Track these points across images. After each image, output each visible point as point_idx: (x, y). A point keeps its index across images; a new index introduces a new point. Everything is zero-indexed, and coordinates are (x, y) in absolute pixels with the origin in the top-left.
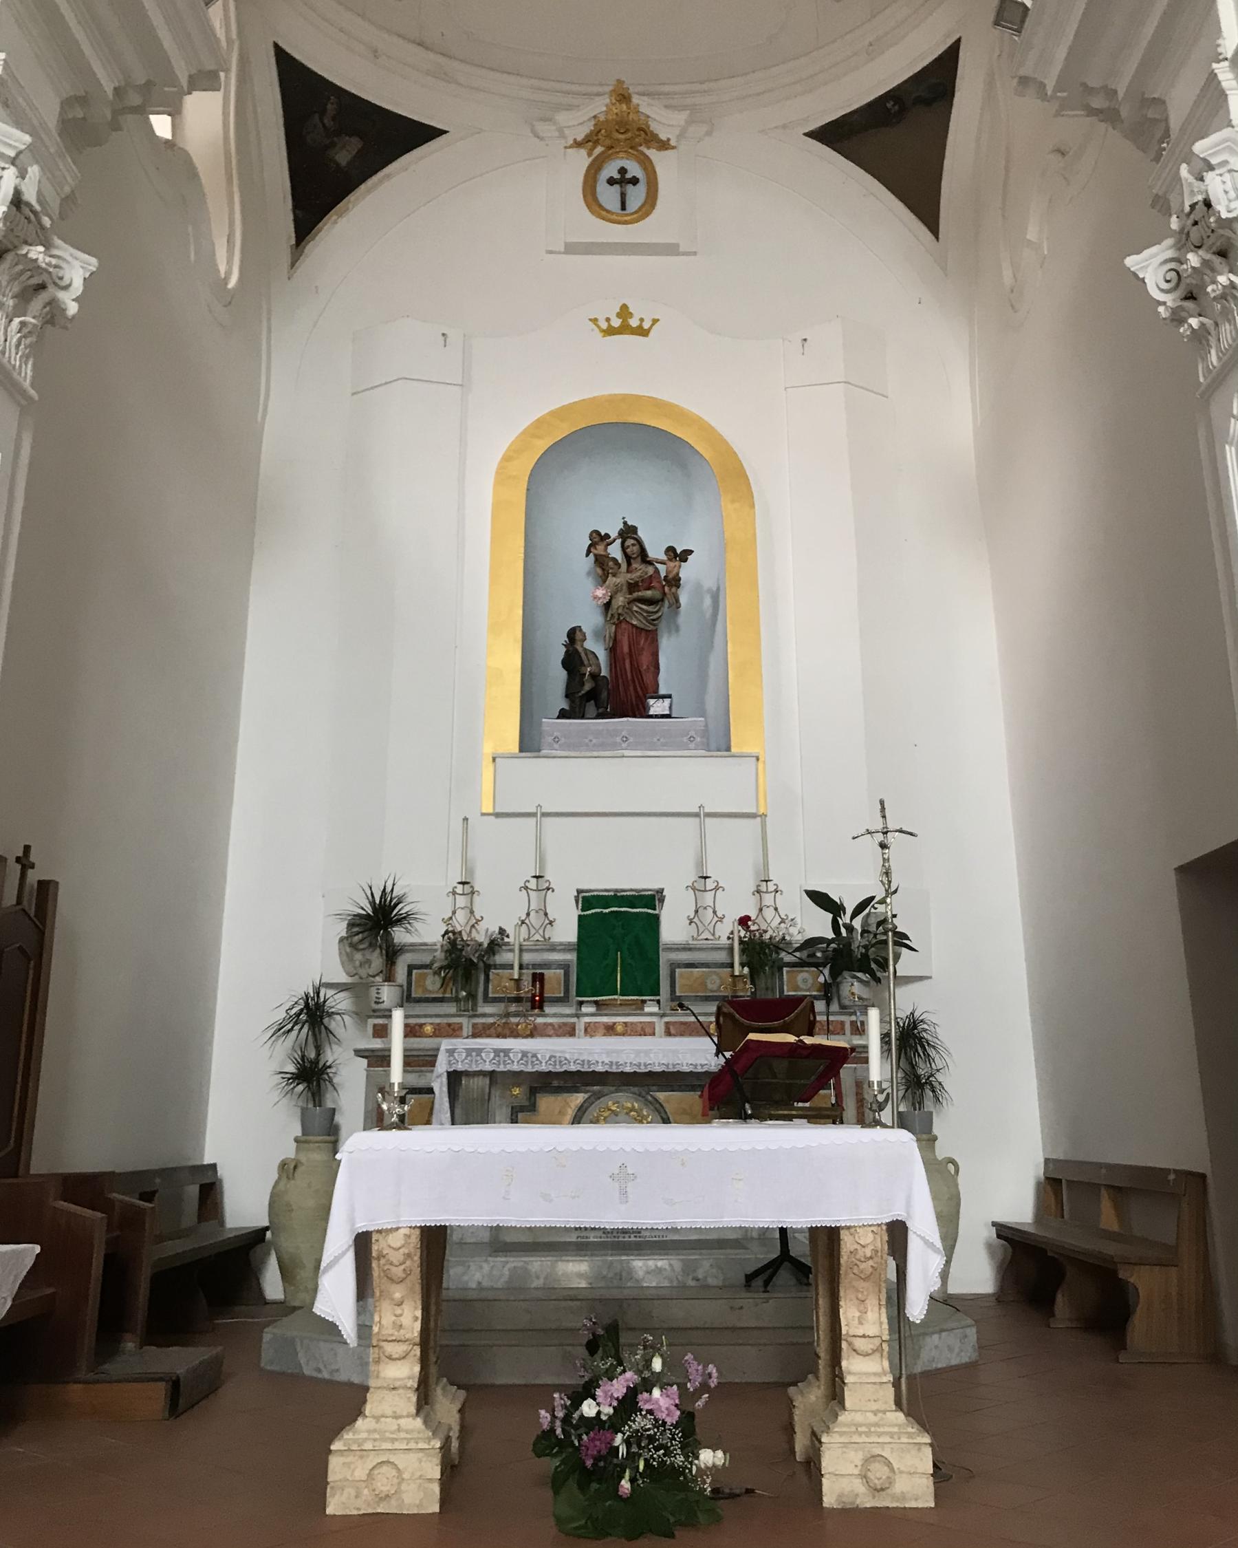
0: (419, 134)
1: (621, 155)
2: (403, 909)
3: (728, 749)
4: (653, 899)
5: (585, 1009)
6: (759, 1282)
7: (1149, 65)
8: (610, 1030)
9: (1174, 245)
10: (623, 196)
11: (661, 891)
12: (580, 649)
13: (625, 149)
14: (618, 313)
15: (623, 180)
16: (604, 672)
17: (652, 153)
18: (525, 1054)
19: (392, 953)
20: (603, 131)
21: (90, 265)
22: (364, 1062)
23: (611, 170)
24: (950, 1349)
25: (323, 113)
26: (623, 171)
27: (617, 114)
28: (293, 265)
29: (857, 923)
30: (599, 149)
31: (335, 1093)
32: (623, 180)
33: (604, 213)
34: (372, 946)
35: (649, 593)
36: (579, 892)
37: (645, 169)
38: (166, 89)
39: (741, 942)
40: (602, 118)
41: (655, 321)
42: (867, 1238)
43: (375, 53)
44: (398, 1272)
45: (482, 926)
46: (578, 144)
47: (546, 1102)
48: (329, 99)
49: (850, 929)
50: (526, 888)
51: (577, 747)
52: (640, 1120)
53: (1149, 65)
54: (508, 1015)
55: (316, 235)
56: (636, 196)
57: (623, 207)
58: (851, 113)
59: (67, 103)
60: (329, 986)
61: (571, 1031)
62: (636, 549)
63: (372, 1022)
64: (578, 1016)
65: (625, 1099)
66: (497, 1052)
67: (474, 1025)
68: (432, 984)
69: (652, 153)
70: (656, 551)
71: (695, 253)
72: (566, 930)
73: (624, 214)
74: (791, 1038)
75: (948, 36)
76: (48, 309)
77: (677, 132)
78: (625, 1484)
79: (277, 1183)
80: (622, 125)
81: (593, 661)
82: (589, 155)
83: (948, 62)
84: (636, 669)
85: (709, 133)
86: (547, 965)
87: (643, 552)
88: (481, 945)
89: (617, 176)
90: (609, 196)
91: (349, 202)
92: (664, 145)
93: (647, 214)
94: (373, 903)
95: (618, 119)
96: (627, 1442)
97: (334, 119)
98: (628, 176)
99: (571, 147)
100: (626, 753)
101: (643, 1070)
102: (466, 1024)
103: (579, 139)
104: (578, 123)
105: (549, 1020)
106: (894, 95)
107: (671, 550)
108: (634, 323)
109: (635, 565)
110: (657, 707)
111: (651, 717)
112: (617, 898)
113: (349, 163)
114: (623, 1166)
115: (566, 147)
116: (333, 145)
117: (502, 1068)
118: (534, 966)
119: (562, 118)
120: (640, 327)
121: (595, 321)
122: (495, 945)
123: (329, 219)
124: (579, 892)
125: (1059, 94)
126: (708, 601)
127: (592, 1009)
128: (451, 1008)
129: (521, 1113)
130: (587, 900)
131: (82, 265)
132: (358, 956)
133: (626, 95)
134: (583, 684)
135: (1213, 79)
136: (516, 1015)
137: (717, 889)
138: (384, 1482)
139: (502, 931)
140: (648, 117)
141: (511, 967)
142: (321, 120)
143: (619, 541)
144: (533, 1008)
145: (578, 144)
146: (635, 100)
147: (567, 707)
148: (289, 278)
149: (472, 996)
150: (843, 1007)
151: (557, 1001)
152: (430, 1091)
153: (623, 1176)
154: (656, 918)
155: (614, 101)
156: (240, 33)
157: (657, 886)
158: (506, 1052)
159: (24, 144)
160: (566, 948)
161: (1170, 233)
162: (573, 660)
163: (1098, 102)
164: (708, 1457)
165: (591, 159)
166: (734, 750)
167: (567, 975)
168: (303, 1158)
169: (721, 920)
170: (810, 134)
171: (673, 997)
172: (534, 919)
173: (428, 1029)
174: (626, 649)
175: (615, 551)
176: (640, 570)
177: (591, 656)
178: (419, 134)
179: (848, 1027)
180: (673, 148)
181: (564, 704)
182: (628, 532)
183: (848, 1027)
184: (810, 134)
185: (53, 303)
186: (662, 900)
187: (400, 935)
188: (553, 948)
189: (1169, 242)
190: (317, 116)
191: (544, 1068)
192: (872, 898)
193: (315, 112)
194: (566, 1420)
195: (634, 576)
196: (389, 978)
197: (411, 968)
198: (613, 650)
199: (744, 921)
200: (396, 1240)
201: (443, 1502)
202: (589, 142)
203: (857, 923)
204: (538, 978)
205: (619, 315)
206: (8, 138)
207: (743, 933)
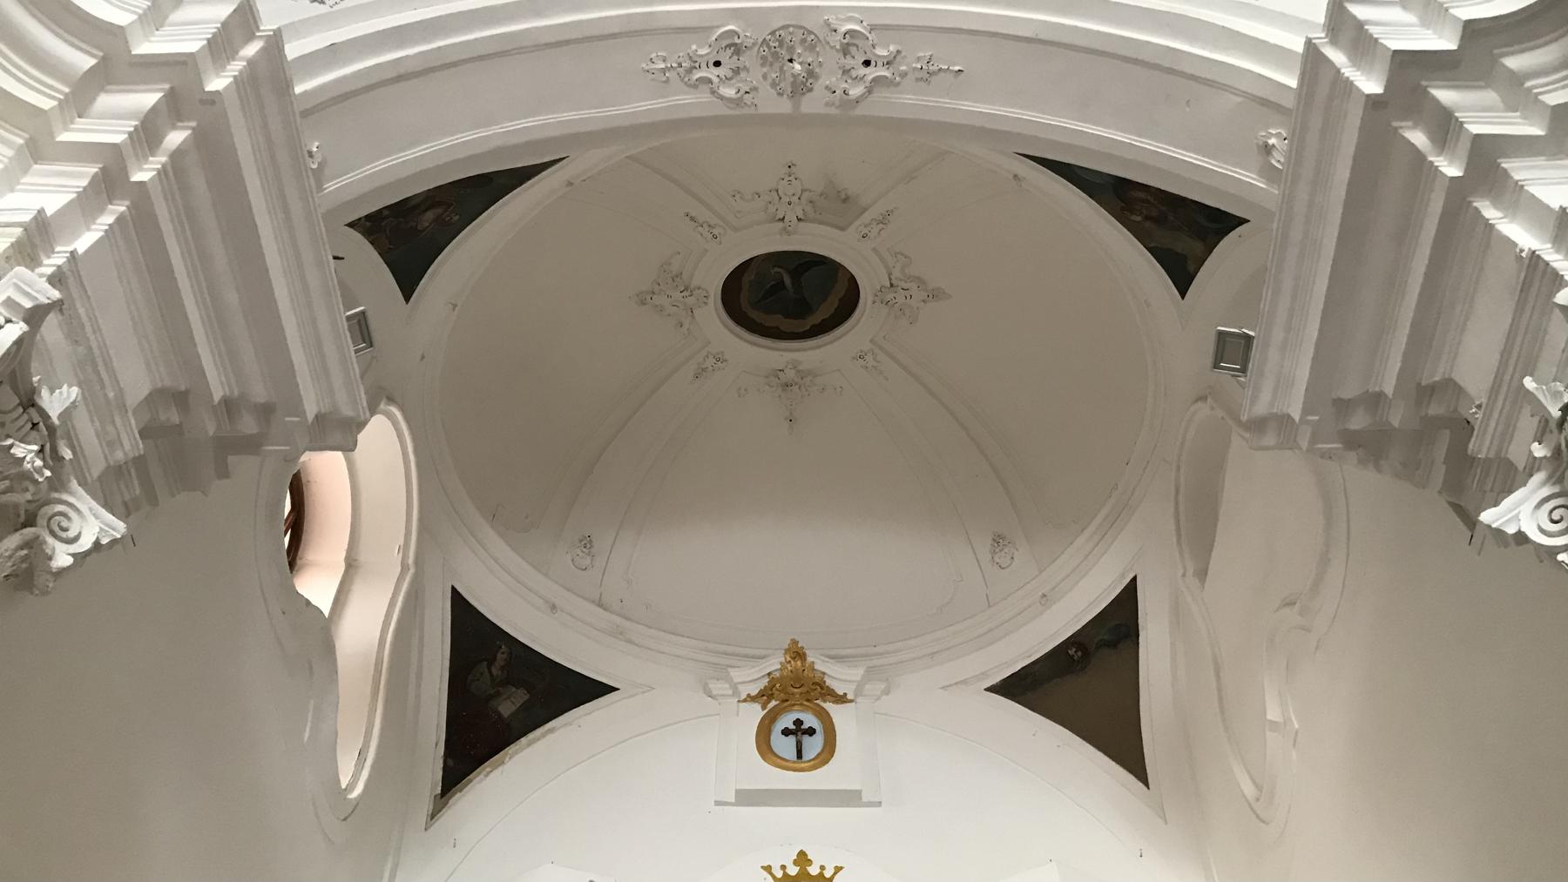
0: (589, 690)
1: (796, 707)
7: (1423, 340)
9: (1549, 478)
13: (801, 701)
14: (795, 860)
15: (799, 731)
20: (778, 686)
21: (114, 529)
23: (787, 721)
25: (491, 663)
26: (798, 722)
27: (791, 671)
28: (433, 816)
30: (773, 703)
32: (799, 731)
33: (779, 760)
38: (287, 419)
40: (778, 674)
41: (838, 869)
43: (554, 607)
46: (751, 699)
48: (500, 647)
53: (1423, 340)
55: (466, 785)
56: (813, 746)
57: (799, 755)
58: (1033, 663)
59: (158, 396)
71: (879, 804)
75: (1123, 576)
76: (25, 552)
77: (853, 687)
82: (764, 708)
83: (1128, 598)
85: (887, 692)
89: (792, 727)
90: (785, 746)
91: (506, 755)
92: (841, 699)
93: (825, 762)
95: (792, 676)
97: (502, 668)
98: (806, 726)
99: (745, 701)
103: (754, 693)
104: (752, 678)
106: (1075, 641)
113: (512, 715)
115: (739, 701)
116: (498, 694)
119: (737, 675)
120: (821, 875)
121: (768, 869)
123: (484, 770)
125: (1310, 418)
131: (103, 526)
133: (801, 652)
135: (1537, 264)
140: (824, 673)
145: (751, 699)
148: (426, 829)
155: (789, 659)
156: (416, 562)
159: (48, 298)
161: (1533, 466)
163: (1358, 421)
165: (765, 711)
170: (991, 689)
178: (589, 690)
180: (851, 701)
184: (991, 689)
185: (33, 545)
189: (1538, 477)
193: (483, 660)
202: (764, 696)
205: (795, 863)
206: (30, 286)
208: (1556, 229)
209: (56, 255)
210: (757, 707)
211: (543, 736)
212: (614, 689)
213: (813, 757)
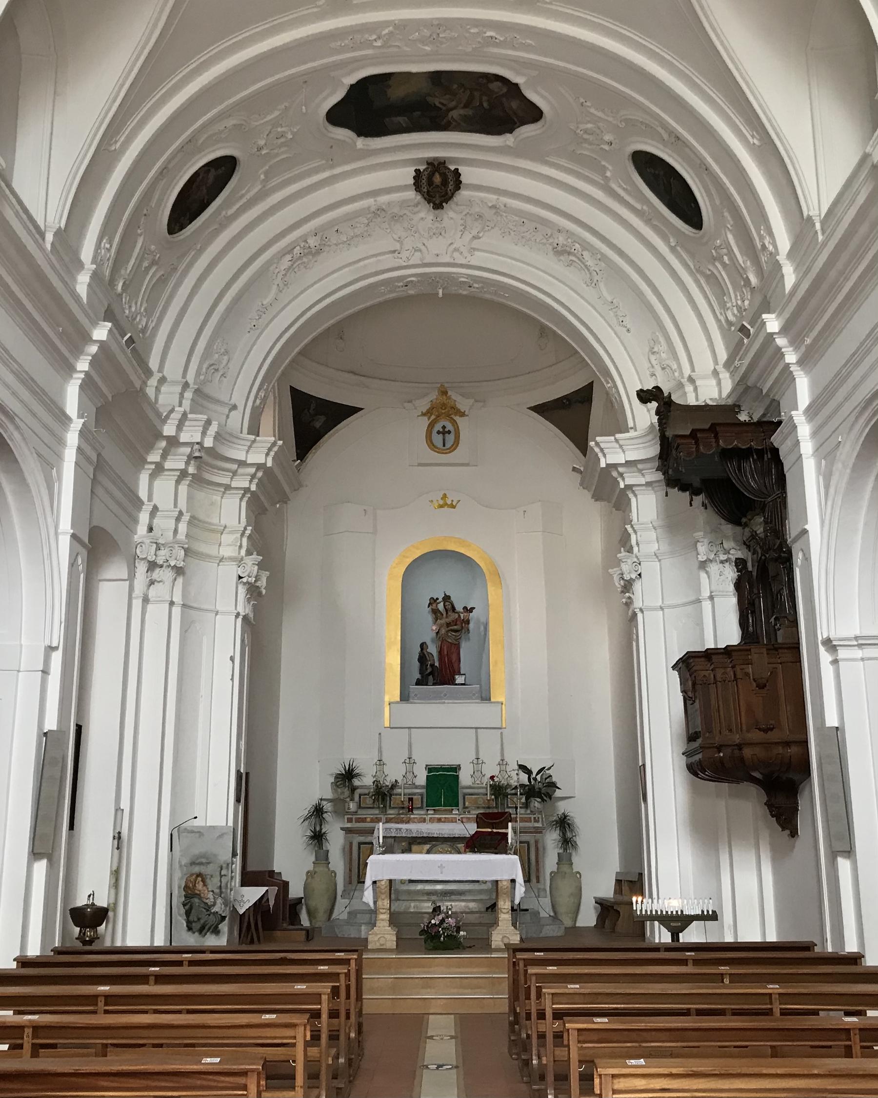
2: (356, 771)
3: (490, 700)
4: (456, 769)
5: (429, 812)
6: (490, 910)
8: (439, 820)
10: (444, 440)
11: (459, 765)
12: (425, 653)
15: (444, 432)
16: (437, 664)
17: (457, 418)
18: (407, 830)
19: (353, 789)
22: (343, 832)
23: (438, 427)
24: (554, 931)
26: (444, 427)
29: (539, 777)
31: (327, 844)
32: (444, 432)
34: (345, 786)
35: (455, 627)
36: (427, 766)
37: (453, 425)
39: (490, 785)
42: (505, 883)
44: (383, 891)
45: (388, 779)
46: (423, 414)
47: (414, 848)
49: (535, 779)
50: (405, 763)
51: (426, 698)
52: (451, 853)
54: (399, 814)
56: (450, 439)
57: (444, 445)
60: (325, 800)
61: (424, 821)
62: (450, 607)
63: (346, 817)
64: (427, 815)
65: (446, 846)
66: (397, 829)
67: (386, 818)
68: (369, 801)
69: (457, 418)
70: (459, 608)
72: (421, 779)
73: (446, 449)
74: (490, 830)
78: (442, 939)
79: (307, 879)
80: (444, 406)
81: (431, 659)
82: (429, 420)
84: (450, 661)
86: (414, 794)
87: (453, 609)
88: (388, 786)
89: (441, 430)
90: (438, 439)
92: (463, 414)
94: (345, 769)
96: (442, 929)
98: (447, 430)
100: (446, 701)
101: (452, 836)
102: (383, 818)
103: (424, 411)
104: (424, 404)
105: (415, 816)
107: (465, 608)
108: (449, 502)
109: (449, 613)
110: (459, 679)
111: (456, 685)
112: (442, 768)
113: (320, 427)
114: (441, 865)
117: (398, 835)
118: (409, 794)
120: (452, 504)
122: (395, 785)
124: (427, 766)
126: (482, 628)
127: (432, 812)
128: (377, 811)
129: (408, 850)
130: (430, 769)
132: (339, 790)
134: (427, 669)
136: (402, 814)
137: (482, 763)
138: (382, 941)
139: (396, 781)
141: (401, 795)
142: (308, 411)
143: (442, 603)
144: (409, 811)
145: (423, 414)
146: (450, 393)
147: (420, 678)
149: (385, 807)
150: (531, 811)
151: (418, 808)
152: (372, 843)
153: (441, 867)
154: (458, 776)
156: (279, 395)
157: (458, 764)
158: (400, 829)
160: (422, 787)
162: (423, 658)
164: (462, 933)
166: (492, 700)
167: (422, 799)
168: (317, 869)
169: (484, 776)
171: (465, 807)
172: (410, 776)
173: (368, 820)
174: (446, 653)
175: (441, 607)
176: (454, 616)
177: (430, 656)
179: (532, 819)
181: (418, 676)
182: (447, 598)
183: (532, 819)
186: (460, 769)
187: (356, 782)
188: (417, 787)
190: (306, 410)
191: (414, 835)
192: (544, 768)
194: (427, 926)
195: (448, 620)
196: (352, 799)
197: (360, 795)
198: (440, 652)
199: (492, 778)
200: (383, 883)
201: (397, 946)
203: (539, 777)
204: (411, 800)
207: (492, 783)
208: (728, 529)
209: (166, 473)
210: (426, 418)
211: (335, 433)
212: (362, 409)
213: (452, 444)
